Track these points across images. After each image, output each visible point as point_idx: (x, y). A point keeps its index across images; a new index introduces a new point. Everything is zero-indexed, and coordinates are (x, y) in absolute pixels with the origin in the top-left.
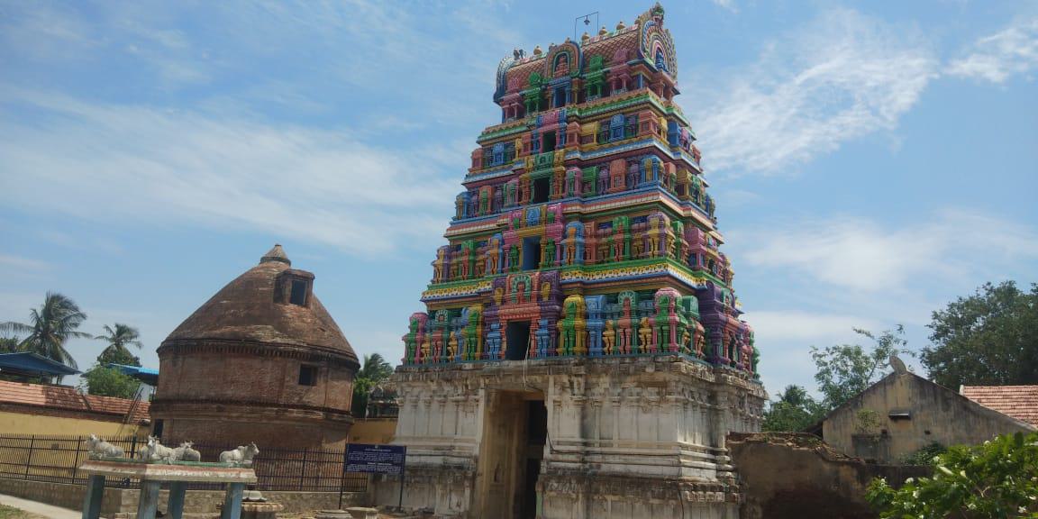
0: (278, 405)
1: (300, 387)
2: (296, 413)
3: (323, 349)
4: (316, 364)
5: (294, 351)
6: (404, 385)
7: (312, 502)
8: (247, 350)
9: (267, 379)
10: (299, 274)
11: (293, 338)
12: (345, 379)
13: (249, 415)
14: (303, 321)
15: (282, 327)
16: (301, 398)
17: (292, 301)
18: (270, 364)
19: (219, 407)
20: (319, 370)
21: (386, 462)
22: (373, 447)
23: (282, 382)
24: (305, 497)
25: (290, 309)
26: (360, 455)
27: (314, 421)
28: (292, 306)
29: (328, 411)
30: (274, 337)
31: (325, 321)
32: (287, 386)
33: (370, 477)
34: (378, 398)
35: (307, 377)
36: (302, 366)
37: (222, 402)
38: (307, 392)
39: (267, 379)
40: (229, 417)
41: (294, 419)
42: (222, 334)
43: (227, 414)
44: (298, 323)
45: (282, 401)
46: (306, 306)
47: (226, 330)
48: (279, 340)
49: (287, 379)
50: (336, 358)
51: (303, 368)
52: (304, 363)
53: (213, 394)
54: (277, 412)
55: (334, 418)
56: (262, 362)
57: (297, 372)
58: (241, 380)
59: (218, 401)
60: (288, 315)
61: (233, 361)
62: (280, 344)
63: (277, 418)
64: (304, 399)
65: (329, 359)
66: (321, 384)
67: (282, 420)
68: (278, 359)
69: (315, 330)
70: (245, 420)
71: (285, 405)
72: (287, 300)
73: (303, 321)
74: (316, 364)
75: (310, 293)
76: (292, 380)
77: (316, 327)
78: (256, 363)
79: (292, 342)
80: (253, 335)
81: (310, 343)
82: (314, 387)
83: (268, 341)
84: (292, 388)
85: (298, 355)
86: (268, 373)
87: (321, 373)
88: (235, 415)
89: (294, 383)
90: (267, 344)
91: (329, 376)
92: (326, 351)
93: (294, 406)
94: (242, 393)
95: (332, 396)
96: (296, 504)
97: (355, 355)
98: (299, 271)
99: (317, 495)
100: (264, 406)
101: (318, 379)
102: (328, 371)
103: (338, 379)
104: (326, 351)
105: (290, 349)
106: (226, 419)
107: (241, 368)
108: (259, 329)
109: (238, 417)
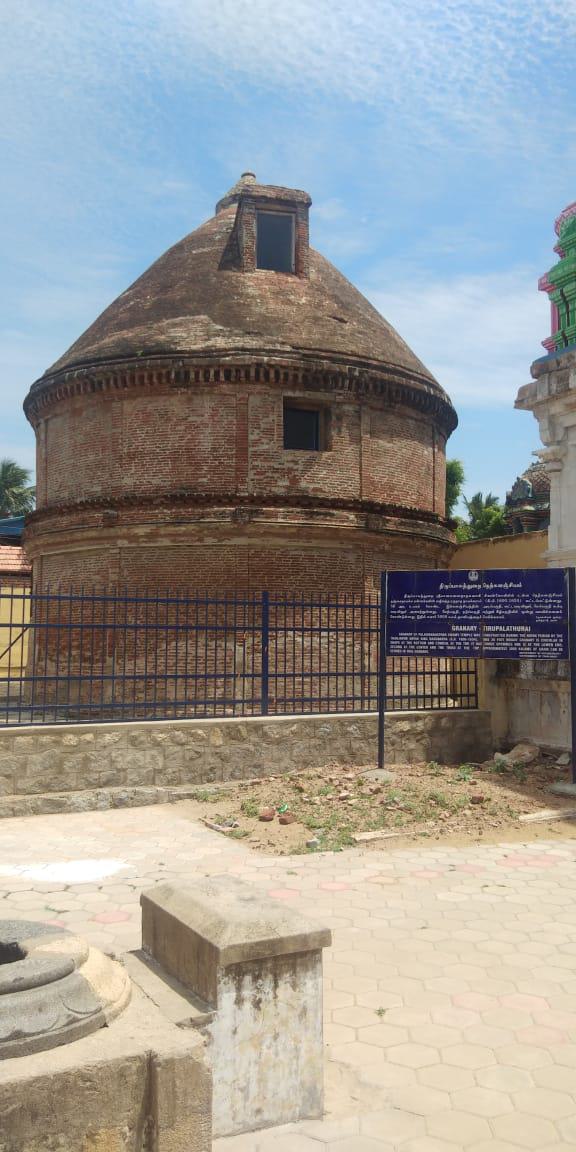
0: (231, 500)
1: (288, 455)
3: (336, 357)
4: (320, 396)
5: (259, 365)
6: (557, 408)
7: (300, 747)
8: (150, 377)
9: (206, 441)
10: (271, 194)
11: (258, 334)
12: (412, 438)
13: (171, 529)
14: (289, 302)
15: (233, 317)
16: (294, 481)
17: (263, 264)
18: (206, 404)
19: (107, 517)
20: (335, 411)
21: (509, 621)
22: (462, 577)
23: (241, 444)
24: (274, 734)
25: (256, 281)
26: (422, 608)
27: (334, 534)
28: (262, 273)
29: (367, 508)
30: (208, 336)
31: (347, 303)
32: (256, 455)
33: (484, 668)
34: (522, 502)
35: (305, 430)
36: (287, 400)
37: (111, 504)
38: (309, 464)
39: (206, 441)
41: (281, 532)
43: (125, 530)
44: (274, 306)
45: (248, 489)
46: (298, 272)
48: (220, 342)
49: (251, 437)
50: (373, 379)
51: (291, 409)
52: (290, 394)
53: (97, 489)
54: (234, 515)
55: (390, 527)
56: (190, 400)
57: (276, 418)
58: (149, 446)
59: (111, 504)
60: (250, 291)
61: (128, 406)
62: (224, 352)
64: (303, 484)
65: (357, 384)
66: (343, 447)
67: (250, 536)
68: (225, 388)
69: (316, 319)
70: (166, 542)
71: (252, 500)
72: (246, 259)
73: (289, 302)
74: (320, 396)
75: (303, 241)
76: (267, 438)
77: (320, 314)
78: (175, 404)
79: (252, 343)
81: (301, 344)
82: (326, 454)
83: (194, 347)
84: (266, 456)
85: (272, 375)
86: (203, 424)
87: (339, 418)
88: (141, 531)
89: (271, 444)
90: (193, 354)
91: (364, 426)
92: (228, 355)
93: (276, 501)
94: (156, 478)
95: (379, 475)
96: (247, 753)
97: (434, 381)
98: (271, 187)
99: (314, 724)
100: (203, 505)
101: (334, 433)
102: (359, 414)
103: (392, 434)
104: (346, 362)
105: (248, 359)
106: (124, 543)
107: (145, 422)
108: (175, 325)
109: (151, 536)
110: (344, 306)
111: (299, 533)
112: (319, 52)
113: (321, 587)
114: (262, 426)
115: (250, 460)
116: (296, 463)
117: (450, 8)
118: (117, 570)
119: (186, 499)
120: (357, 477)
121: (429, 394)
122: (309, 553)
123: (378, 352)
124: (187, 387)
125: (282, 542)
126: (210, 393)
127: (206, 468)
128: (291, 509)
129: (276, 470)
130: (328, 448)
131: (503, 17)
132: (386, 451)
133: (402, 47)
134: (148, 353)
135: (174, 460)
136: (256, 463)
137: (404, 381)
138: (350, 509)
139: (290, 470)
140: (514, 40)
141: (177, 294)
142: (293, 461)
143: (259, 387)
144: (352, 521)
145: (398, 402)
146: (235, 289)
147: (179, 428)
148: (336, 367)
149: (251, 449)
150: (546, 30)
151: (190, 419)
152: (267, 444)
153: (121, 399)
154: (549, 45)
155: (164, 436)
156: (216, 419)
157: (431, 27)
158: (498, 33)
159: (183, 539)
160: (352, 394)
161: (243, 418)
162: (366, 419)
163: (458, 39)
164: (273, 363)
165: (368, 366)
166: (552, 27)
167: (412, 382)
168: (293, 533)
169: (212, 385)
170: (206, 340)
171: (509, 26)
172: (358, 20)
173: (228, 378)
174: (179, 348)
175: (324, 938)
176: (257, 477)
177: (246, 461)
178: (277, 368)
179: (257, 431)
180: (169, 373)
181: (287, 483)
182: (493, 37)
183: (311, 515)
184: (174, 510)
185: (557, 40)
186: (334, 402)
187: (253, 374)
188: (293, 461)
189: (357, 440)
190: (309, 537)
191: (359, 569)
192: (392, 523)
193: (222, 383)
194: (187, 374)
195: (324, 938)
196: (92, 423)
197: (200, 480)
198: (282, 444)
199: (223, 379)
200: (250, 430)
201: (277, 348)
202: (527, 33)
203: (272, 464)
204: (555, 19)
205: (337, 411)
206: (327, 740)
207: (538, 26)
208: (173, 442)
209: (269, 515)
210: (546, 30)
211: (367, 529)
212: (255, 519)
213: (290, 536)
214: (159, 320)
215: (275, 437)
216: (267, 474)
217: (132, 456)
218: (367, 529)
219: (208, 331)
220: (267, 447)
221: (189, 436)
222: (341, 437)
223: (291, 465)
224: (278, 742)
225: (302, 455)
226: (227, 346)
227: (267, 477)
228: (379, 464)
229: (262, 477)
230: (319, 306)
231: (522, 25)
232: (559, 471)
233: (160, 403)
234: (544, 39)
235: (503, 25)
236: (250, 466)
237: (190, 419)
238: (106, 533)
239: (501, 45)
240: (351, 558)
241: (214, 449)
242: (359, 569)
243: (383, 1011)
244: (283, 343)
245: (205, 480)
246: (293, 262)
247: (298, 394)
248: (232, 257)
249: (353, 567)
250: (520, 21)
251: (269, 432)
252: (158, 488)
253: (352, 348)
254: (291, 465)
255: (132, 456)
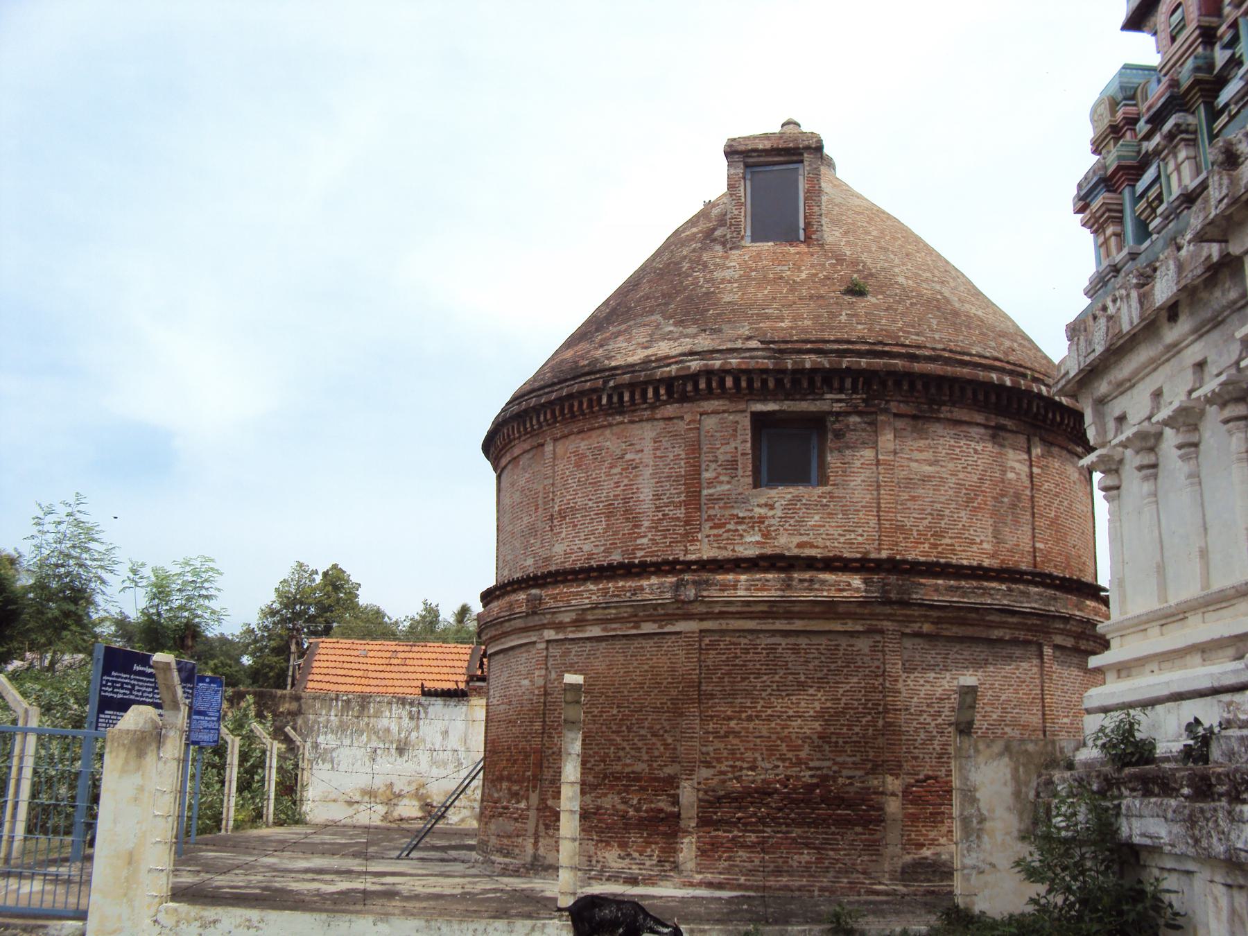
10: (767, 145)
18: (646, 434)
27: (829, 609)
32: (713, 500)
36: (757, 418)
48: (664, 348)
49: (706, 475)
52: (759, 407)
83: (630, 360)
84: (725, 500)
85: (729, 382)
106: (550, 634)
113: (811, 691)
114: (721, 458)
115: (704, 507)
116: (772, 507)
118: (543, 672)
120: (873, 522)
121: (1002, 386)
122: (792, 640)
123: (935, 335)
124: (622, 413)
126: (651, 419)
127: (646, 524)
128: (758, 576)
129: (741, 521)
130: (823, 480)
135: (609, 515)
136: (711, 512)
137: (879, 362)
138: (855, 571)
139: (762, 520)
142: (766, 505)
143: (714, 404)
144: (857, 590)
145: (944, 403)
147: (614, 471)
149: (705, 492)
151: (628, 457)
152: (728, 483)
155: (596, 484)
156: (658, 453)
159: (614, 626)
160: (858, 398)
161: (695, 448)
164: (728, 367)
167: (994, 376)
168: (762, 612)
169: (653, 407)
170: (646, 348)
173: (670, 393)
174: (613, 364)
176: (715, 532)
177: (699, 509)
178: (737, 374)
179: (713, 466)
180: (600, 399)
181: (758, 538)
184: (601, 586)
186: (831, 413)
187: (702, 385)
188: (766, 505)
190: (790, 616)
191: (877, 663)
193: (665, 403)
196: (527, 475)
197: (639, 542)
198: (750, 480)
199: (664, 398)
200: (704, 467)
203: (735, 512)
205: (837, 426)
208: (608, 489)
209: (724, 587)
212: (705, 593)
215: (740, 472)
216: (728, 527)
217: (562, 515)
220: (727, 487)
221: (626, 481)
223: (763, 511)
226: (674, 352)
227: (728, 531)
228: (913, 498)
229: (721, 531)
232: (1118, 488)
236: (705, 516)
237: (628, 457)
241: (657, 497)
242: (877, 663)
244: (749, 338)
245: (645, 541)
246: (802, 225)
247: (771, 407)
249: (866, 659)
251: (732, 465)
254: (763, 511)
255: (562, 515)
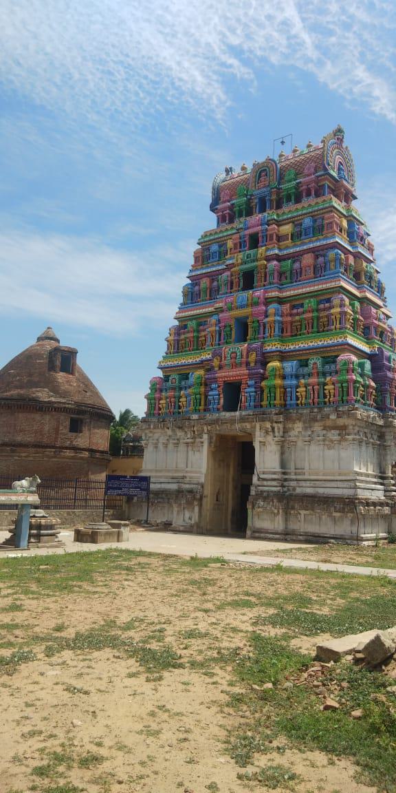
0: (53, 447)
1: (70, 434)
2: (68, 453)
3: (87, 405)
4: (81, 417)
5: (65, 408)
9: (46, 428)
15: (55, 390)
16: (72, 442)
18: (47, 417)
20: (84, 421)
22: (125, 477)
23: (57, 430)
24: (77, 514)
25: (61, 376)
27: (82, 458)
29: (91, 451)
31: (87, 385)
32: (61, 433)
33: (124, 498)
35: (75, 427)
37: (14, 446)
39: (46, 428)
40: (19, 456)
42: (12, 395)
43: (18, 454)
45: (58, 444)
46: (72, 373)
47: (14, 392)
48: (53, 399)
53: (6, 440)
54: (55, 452)
56: (42, 416)
57: (68, 423)
61: (20, 415)
63: (55, 457)
70: (32, 459)
71: (60, 448)
72: (58, 369)
73: (71, 386)
74: (81, 417)
75: (74, 364)
77: (80, 390)
78: (37, 416)
79: (63, 400)
80: (34, 395)
88: (23, 455)
89: (66, 431)
94: (29, 438)
103: (99, 427)
106: (17, 458)
108: (38, 391)
110: (86, 386)
111: (73, 458)
112: (19, 64)
117: (112, 60)
119: (38, 446)
125: (67, 460)
131: (146, 77)
132: (97, 433)
133: (77, 76)
134: (30, 400)
140: (148, 93)
141: (36, 379)
146: (55, 380)
148: (86, 409)
150: (171, 93)
153: (18, 412)
154: (172, 104)
157: (98, 69)
158: (140, 87)
162: (92, 423)
163: (114, 82)
165: (94, 408)
166: (174, 92)
171: (148, 84)
172: (49, 49)
173: (55, 410)
175: (357, 198)
178: (70, 409)
182: (137, 88)
183: (76, 453)
185: (176, 101)
189: (89, 430)
192: (98, 455)
194: (42, 408)
195: (357, 198)
201: (68, 401)
202: (159, 92)
204: (176, 89)
206: (89, 516)
207: (167, 90)
210: (171, 93)
211: (91, 457)
213: (70, 459)
214: (31, 388)
217: (21, 431)
218: (91, 457)
219: (384, 789)
222: (85, 429)
224: (78, 516)
225: (74, 434)
230: (79, 386)
231: (157, 86)
233: (33, 415)
234: (169, 98)
235: (144, 81)
238: (11, 454)
239: (142, 95)
240: (86, 465)
241: (49, 431)
243: (283, 144)
248: (52, 367)
250: (157, 83)
252: (30, 442)
253: (90, 402)
